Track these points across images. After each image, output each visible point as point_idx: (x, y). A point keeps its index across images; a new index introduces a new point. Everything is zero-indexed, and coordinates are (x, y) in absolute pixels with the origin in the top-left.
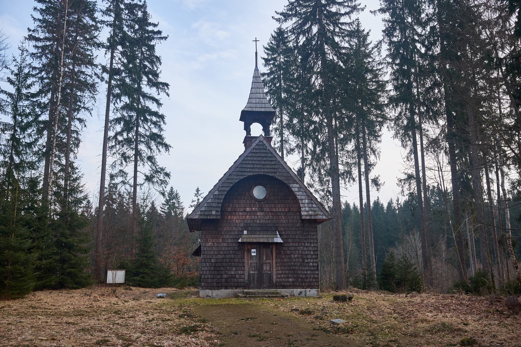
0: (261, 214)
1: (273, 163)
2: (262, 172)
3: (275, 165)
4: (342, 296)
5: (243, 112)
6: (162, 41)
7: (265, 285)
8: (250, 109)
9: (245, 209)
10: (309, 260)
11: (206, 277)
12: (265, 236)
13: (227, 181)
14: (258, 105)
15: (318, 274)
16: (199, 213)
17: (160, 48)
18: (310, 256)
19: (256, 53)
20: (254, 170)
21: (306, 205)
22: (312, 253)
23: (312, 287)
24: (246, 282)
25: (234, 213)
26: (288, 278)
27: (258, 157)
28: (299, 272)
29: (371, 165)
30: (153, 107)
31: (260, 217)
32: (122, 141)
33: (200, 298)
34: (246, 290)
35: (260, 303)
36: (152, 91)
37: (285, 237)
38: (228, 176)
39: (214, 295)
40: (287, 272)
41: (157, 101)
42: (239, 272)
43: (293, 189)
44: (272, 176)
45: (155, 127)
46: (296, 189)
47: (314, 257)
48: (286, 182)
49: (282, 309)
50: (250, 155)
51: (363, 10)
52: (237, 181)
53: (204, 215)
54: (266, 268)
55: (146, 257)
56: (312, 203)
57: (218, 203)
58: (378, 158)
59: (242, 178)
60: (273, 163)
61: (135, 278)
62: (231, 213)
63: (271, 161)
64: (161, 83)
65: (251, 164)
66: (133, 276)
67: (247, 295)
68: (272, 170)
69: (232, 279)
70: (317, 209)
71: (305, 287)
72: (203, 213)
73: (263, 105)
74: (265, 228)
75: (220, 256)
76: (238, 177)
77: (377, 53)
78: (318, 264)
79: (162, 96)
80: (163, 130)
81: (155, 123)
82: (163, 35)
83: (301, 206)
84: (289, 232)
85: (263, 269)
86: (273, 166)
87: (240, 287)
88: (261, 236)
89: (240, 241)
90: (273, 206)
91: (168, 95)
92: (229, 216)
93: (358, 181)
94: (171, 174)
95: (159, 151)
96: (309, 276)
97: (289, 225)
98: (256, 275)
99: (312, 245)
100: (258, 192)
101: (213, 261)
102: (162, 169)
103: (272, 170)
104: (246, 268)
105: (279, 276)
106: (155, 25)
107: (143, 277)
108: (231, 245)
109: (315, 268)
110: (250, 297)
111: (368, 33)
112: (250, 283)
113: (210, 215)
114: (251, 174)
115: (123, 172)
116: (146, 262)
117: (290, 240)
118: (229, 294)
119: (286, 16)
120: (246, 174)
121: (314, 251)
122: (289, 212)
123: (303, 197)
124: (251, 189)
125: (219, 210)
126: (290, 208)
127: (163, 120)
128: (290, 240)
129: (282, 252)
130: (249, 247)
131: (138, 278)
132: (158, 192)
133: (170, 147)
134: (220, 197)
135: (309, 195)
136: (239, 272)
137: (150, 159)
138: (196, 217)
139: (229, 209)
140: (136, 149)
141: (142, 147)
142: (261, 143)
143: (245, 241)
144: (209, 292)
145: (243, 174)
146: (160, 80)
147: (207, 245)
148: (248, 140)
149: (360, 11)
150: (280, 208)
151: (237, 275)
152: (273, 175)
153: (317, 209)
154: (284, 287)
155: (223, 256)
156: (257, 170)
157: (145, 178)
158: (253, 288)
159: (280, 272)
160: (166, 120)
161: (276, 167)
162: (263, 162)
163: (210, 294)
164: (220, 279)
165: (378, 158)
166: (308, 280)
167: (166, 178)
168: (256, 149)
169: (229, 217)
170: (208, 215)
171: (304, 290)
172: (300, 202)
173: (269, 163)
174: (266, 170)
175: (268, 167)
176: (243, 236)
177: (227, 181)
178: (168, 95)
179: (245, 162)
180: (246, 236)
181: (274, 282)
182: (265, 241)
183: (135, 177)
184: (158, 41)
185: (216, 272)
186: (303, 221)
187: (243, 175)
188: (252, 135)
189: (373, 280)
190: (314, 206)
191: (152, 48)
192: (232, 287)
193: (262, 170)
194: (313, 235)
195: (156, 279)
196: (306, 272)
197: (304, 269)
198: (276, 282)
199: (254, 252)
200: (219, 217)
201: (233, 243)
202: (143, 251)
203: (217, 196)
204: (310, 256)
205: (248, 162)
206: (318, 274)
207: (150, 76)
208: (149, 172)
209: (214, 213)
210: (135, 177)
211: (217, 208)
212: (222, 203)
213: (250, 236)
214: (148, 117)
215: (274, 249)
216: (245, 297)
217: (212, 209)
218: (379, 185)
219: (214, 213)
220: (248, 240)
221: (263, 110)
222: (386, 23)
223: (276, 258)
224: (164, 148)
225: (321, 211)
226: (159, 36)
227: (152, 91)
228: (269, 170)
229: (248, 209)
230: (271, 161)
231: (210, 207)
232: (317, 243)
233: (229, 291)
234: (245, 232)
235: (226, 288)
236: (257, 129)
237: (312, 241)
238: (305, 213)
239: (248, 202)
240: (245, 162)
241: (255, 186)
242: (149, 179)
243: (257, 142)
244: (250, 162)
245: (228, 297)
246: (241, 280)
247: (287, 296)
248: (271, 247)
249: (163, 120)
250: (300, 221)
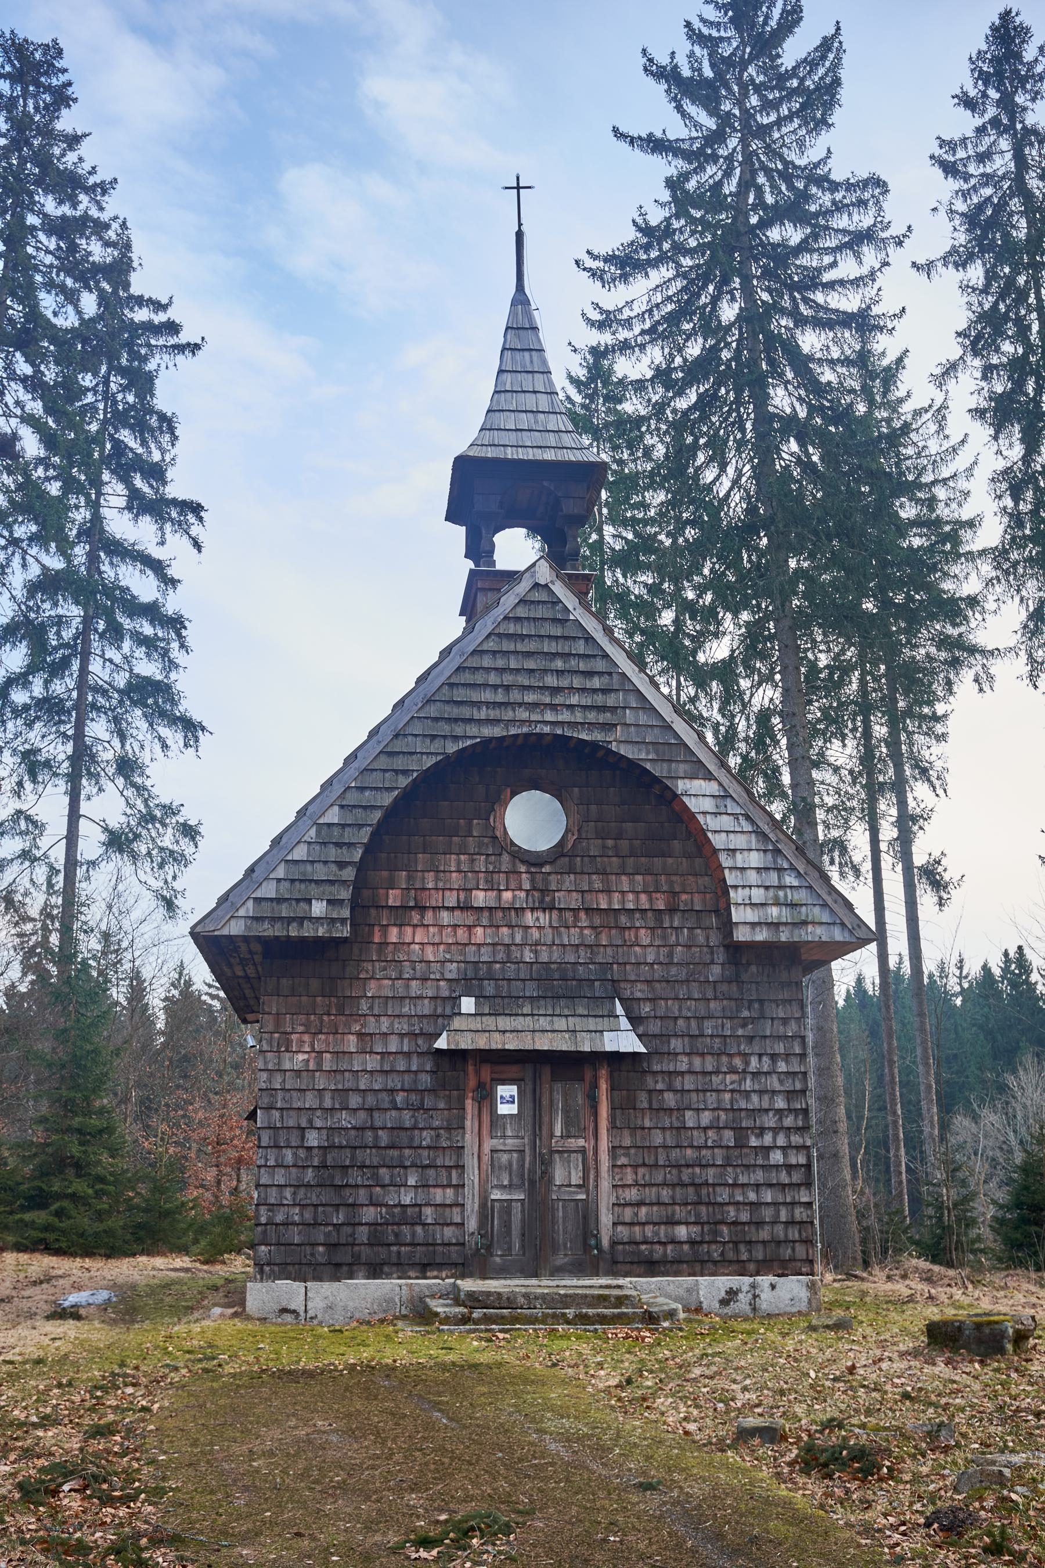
0: (544, 918)
1: (596, 683)
2: (546, 722)
3: (605, 691)
4: (978, 1326)
5: (463, 466)
6: (180, 358)
7: (560, 1260)
8: (490, 453)
9: (468, 898)
10: (768, 1139)
11: (279, 1218)
12: (561, 1024)
13: (383, 762)
14: (527, 439)
15: (809, 1204)
16: (249, 909)
17: (174, 385)
18: (770, 1121)
19: (519, 236)
20: (509, 715)
21: (753, 877)
22: (780, 1103)
23: (784, 1268)
24: (472, 1242)
25: (416, 917)
26: (672, 1222)
27: (529, 654)
28: (723, 1195)
29: (914, 819)
30: (143, 586)
31: (535, 934)
32: (26, 708)
33: (249, 1318)
34: (468, 1285)
35: (538, 1365)
36: (141, 532)
37: (654, 1027)
38: (388, 740)
39: (316, 1305)
40: (665, 1194)
41: (157, 567)
42: (438, 1195)
43: (692, 804)
44: (594, 745)
45: (148, 655)
46: (708, 805)
47: (789, 1121)
48: (656, 770)
49: (670, 1411)
50: (491, 645)
51: (900, 243)
52: (429, 762)
53: (273, 919)
54: (565, 1174)
55: (79, 1131)
56: (780, 870)
57: (341, 865)
58: (940, 792)
59: (452, 748)
60: (596, 683)
61: (28, 1216)
62: (401, 914)
63: (589, 674)
64: (174, 502)
65: (495, 687)
66: (23, 1209)
67: (478, 1312)
68: (592, 716)
69: (405, 1229)
70: (801, 896)
71: (752, 1267)
72: (266, 910)
73: (552, 440)
74: (561, 987)
75: (345, 1119)
76: (436, 746)
77: (933, 427)
78: (809, 1157)
79: (174, 549)
80: (177, 666)
81: (148, 643)
82: (183, 338)
83: (730, 882)
84: (674, 1007)
85: (551, 1180)
86: (599, 699)
87: (440, 1266)
88: (543, 1023)
89: (442, 1043)
90: (598, 885)
91: (197, 545)
92: (394, 931)
93: (870, 876)
94: (201, 829)
95: (165, 746)
96: (767, 1214)
97: (674, 971)
98: (517, 1208)
99: (782, 1067)
100: (532, 820)
101: (313, 1139)
102: (170, 810)
103: (592, 716)
104: (472, 1175)
105: (628, 1214)
106: (159, 306)
107: (59, 1214)
108: (401, 1065)
109: (797, 1177)
110: (487, 1319)
111: (900, 360)
112: (489, 1248)
113: (301, 920)
114: (497, 732)
115: (28, 818)
116: (75, 1150)
117: (676, 1044)
118: (389, 1301)
119: (626, 264)
120: (472, 730)
121: (790, 1095)
122: (672, 910)
123: (738, 841)
124: (496, 802)
125: (345, 894)
127: (180, 636)
128: (676, 1044)
130: (486, 1074)
131: (40, 1217)
132: (149, 895)
133: (203, 729)
134: (348, 836)
135: (766, 828)
136: (438, 1195)
137: (127, 767)
138: (236, 928)
139: (394, 898)
140: (79, 736)
141: (98, 728)
142: (543, 596)
143: (465, 1043)
144: (289, 1291)
145: (459, 730)
146: (174, 490)
147: (287, 1066)
148: (484, 584)
150: (627, 894)
151: (428, 1211)
152: (597, 736)
153: (801, 896)
154: (652, 1267)
155: (362, 1115)
156: (523, 714)
157: (103, 837)
158: (503, 1272)
159: (632, 1194)
160: (190, 633)
161: (611, 701)
162: (551, 681)
163: (297, 1304)
164: (348, 1229)
165: (940, 792)
166: (764, 1234)
167: (185, 846)
168: (518, 619)
169: (393, 934)
170: (290, 920)
171: (747, 1280)
172: (725, 860)
173: (577, 682)
174: (565, 716)
175: (574, 700)
176: (457, 1023)
177: (383, 762)
178: (197, 545)
179: (467, 677)
180: (470, 1027)
181: (605, 1243)
182: (562, 1044)
183: (72, 838)
184: (166, 357)
185: (327, 1196)
186: (737, 952)
187: (456, 738)
188: (500, 566)
189: (971, 1223)
190: (790, 880)
191: (143, 383)
192: (400, 1267)
193: (549, 716)
194: (785, 1021)
195: (116, 1222)
196: (752, 1196)
197: (742, 1179)
198: (614, 1243)
199: (507, 1100)
200: (345, 931)
201: (408, 1055)
202: (68, 1106)
203: (336, 831)
204: (770, 1121)
205: (479, 678)
206: (809, 1204)
207: (138, 482)
208: (123, 819)
209: (318, 908)
210: (72, 838)
211: (334, 889)
212: (361, 867)
213: (490, 1022)
214: (126, 623)
215: (603, 1086)
216: (465, 1320)
217: (314, 890)
218: (945, 887)
219: (318, 908)
220: (482, 1043)
221: (549, 456)
222: (974, 299)
223: (613, 1126)
224: (180, 737)
225: (825, 905)
226: (172, 341)
227: (141, 532)
228: (579, 717)
229: (480, 898)
230: (589, 674)
231: (301, 883)
232: (803, 1056)
233: (389, 1288)
234: (468, 1004)
235: (375, 1271)
236: (516, 549)
237: (780, 1048)
238: (750, 915)
239: (481, 863)
240: (467, 677)
241: (514, 794)
242: (118, 842)
243: (523, 587)
244: (493, 679)
245: (382, 1320)
246: (449, 1232)
247: (671, 1314)
248: (588, 1075)
249: (180, 636)
250: (720, 956)
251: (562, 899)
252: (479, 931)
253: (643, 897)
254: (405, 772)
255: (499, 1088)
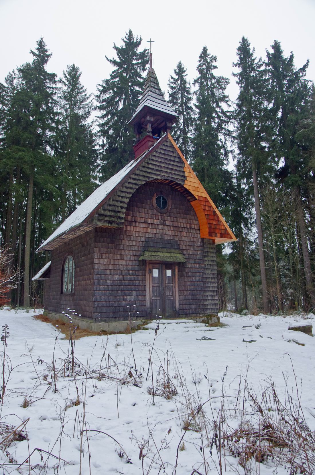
25: (134, 224)
52: (144, 183)
92: (129, 227)
98: (158, 301)
114: (159, 178)
120: (153, 176)
122: (191, 228)
126: (191, 224)
129: (185, 273)
130: (151, 266)
149: (199, 59)
181: (177, 309)
193: (170, 176)
215: (177, 271)
229: (150, 221)
251: (168, 223)
252: (149, 229)
253: (185, 224)
254: (137, 185)
255: (157, 270)
